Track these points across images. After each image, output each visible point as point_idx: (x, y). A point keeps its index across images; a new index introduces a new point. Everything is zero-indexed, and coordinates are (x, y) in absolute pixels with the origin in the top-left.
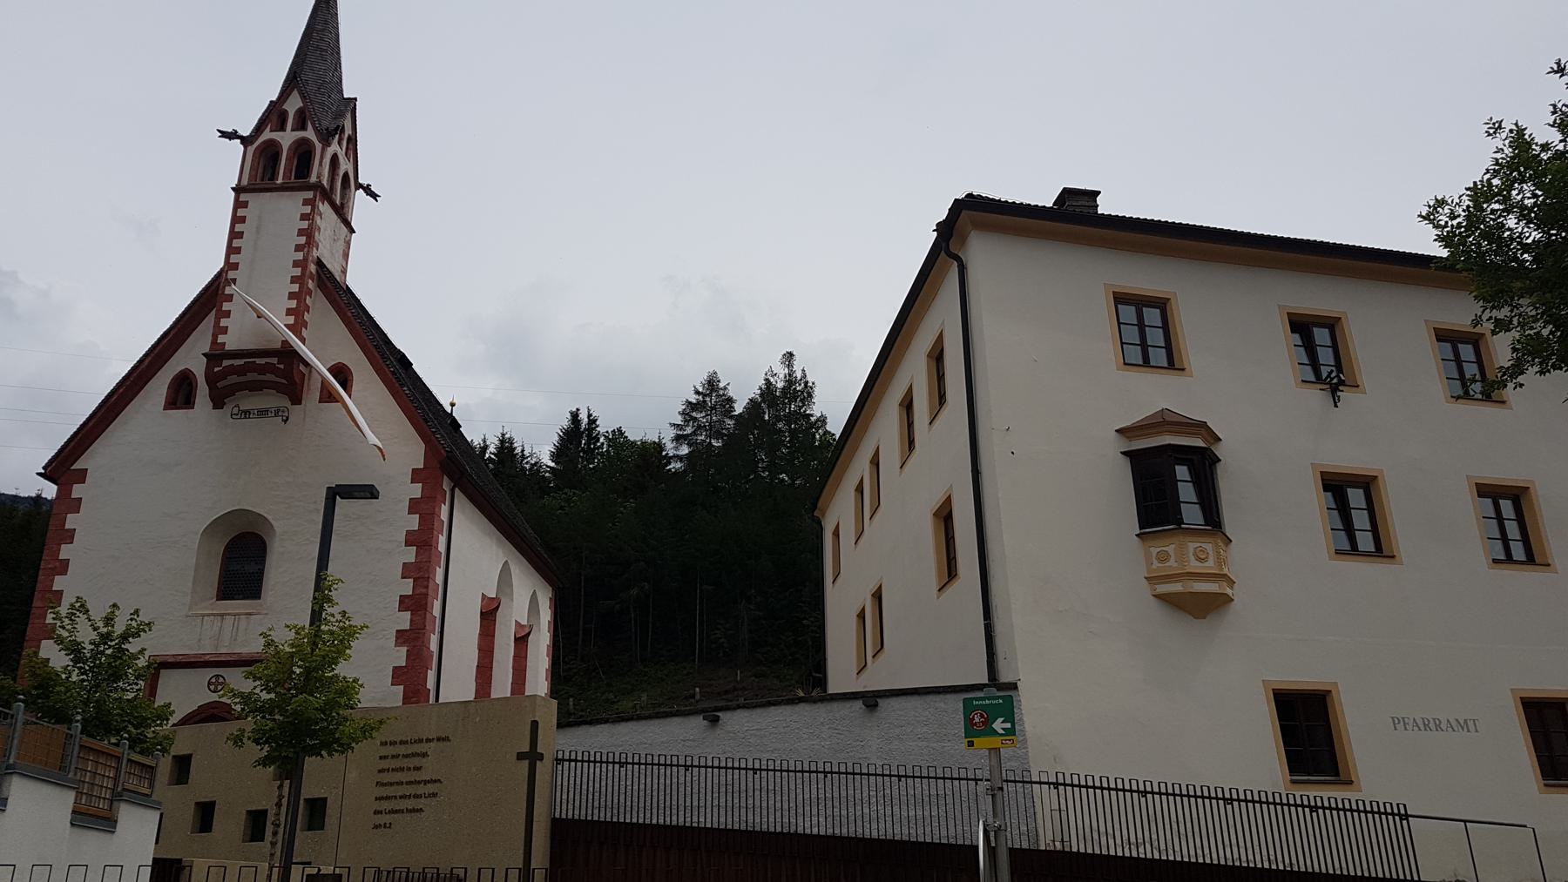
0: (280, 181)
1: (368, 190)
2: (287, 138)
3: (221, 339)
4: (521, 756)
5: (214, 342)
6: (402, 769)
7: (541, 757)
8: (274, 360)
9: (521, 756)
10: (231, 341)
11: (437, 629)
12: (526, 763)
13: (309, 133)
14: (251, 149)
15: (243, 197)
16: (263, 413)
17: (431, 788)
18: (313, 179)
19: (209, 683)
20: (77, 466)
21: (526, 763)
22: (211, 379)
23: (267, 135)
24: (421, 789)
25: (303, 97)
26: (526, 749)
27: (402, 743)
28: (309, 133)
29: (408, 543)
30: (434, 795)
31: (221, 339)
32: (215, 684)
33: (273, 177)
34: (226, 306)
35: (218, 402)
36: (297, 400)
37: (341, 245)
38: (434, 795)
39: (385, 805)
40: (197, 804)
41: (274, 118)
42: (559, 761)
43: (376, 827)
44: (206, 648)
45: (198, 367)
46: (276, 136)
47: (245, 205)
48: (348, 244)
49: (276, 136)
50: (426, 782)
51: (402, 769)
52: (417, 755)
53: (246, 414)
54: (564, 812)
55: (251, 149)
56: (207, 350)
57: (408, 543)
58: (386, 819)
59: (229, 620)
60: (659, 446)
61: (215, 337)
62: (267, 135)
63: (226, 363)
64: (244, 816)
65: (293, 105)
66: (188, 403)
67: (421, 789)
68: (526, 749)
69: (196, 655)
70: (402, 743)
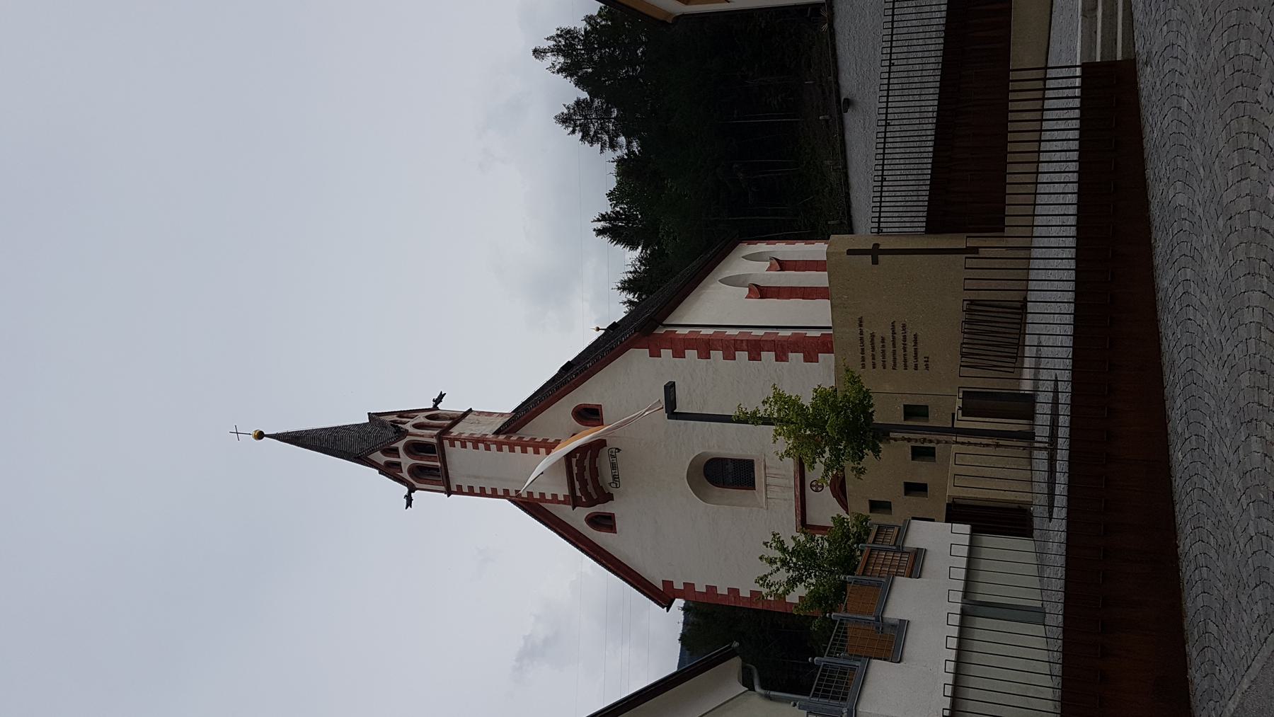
3: (561, 498)
4: (875, 262)
5: (563, 503)
7: (876, 245)
9: (875, 262)
10: (563, 491)
13: (400, 445)
14: (417, 485)
15: (454, 489)
16: (614, 466)
17: (899, 329)
18: (434, 441)
24: (899, 337)
27: (863, 351)
28: (400, 445)
30: (904, 326)
31: (561, 498)
32: (817, 487)
33: (437, 469)
34: (536, 496)
35: (609, 497)
38: (904, 326)
50: (894, 333)
53: (615, 478)
55: (417, 485)
56: (570, 507)
59: (770, 480)
60: (620, 162)
61: (560, 502)
63: (579, 494)
66: (610, 517)
67: (899, 337)
70: (863, 351)
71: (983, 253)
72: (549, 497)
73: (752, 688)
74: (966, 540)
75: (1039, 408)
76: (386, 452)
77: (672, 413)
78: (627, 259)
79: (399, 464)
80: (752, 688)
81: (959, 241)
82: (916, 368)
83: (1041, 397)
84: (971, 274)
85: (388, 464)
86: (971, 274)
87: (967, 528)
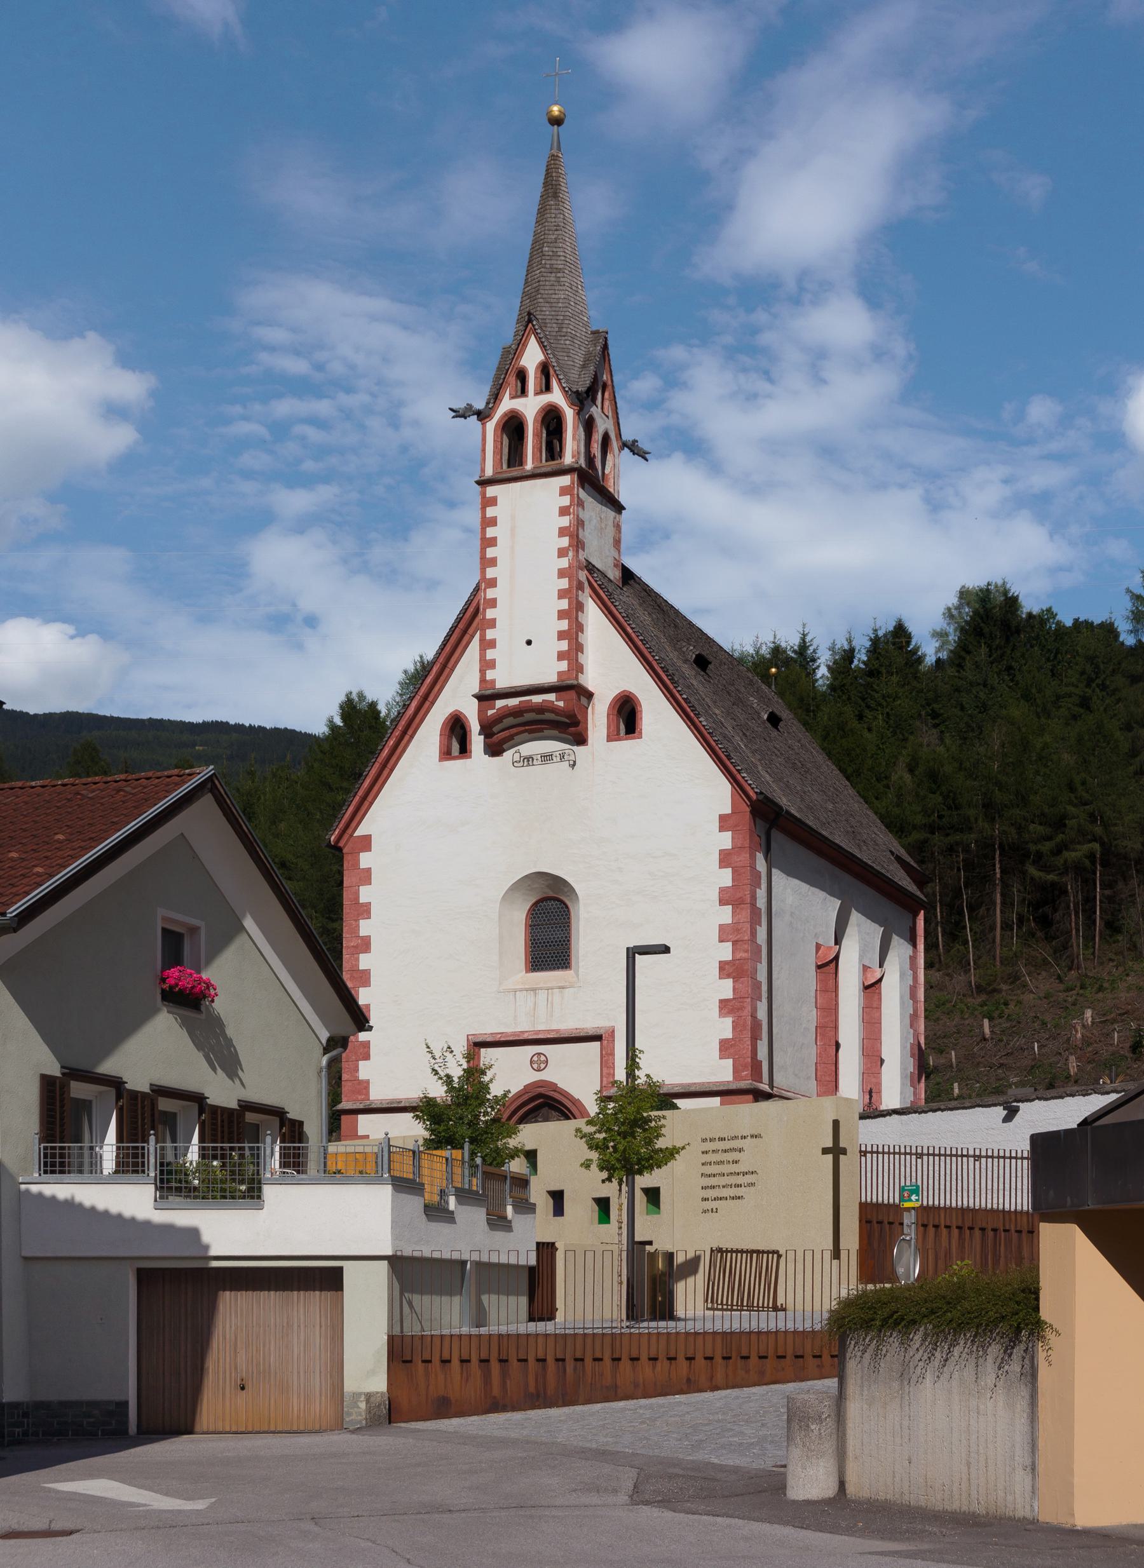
0: (529, 465)
1: (633, 447)
2: (530, 407)
3: (490, 675)
4: (825, 1151)
5: (483, 680)
6: (722, 1162)
7: (844, 1151)
8: (551, 697)
9: (825, 1151)
10: (502, 679)
11: (765, 995)
12: (830, 1156)
13: (557, 397)
14: (491, 425)
15: (491, 491)
16: (547, 758)
17: (749, 1179)
18: (568, 459)
19: (531, 1062)
20: (359, 832)
21: (830, 1156)
22: (487, 729)
23: (507, 404)
24: (740, 1180)
25: (543, 347)
26: (830, 1144)
27: (722, 1139)
28: (557, 397)
29: (722, 902)
30: (753, 1184)
31: (490, 675)
32: (539, 1063)
33: (521, 463)
34: (490, 634)
35: (494, 750)
36: (580, 740)
37: (610, 531)
38: (753, 1184)
39: (711, 1193)
40: (370, 836)
41: (512, 379)
42: (864, 1153)
43: (705, 1212)
44: (523, 1026)
45: (471, 713)
46: (519, 404)
47: (493, 502)
48: (618, 527)
49: (519, 404)
50: (745, 1173)
51: (722, 1162)
52: (734, 1150)
53: (529, 760)
54: (873, 1197)
55: (491, 425)
56: (476, 690)
57: (722, 902)
58: (714, 1205)
59: (542, 995)
60: (1108, 630)
61: (483, 673)
62: (507, 404)
63: (500, 703)
64: (590, 741)
65: (532, 357)
66: (464, 750)
67: (740, 1180)
68: (830, 1144)
69: (514, 1034)
70: (722, 1139)
71: (835, 1262)
72: (490, 654)
73: (326, 1050)
74: (523, 1262)
75: (662, 1324)
76: (545, 370)
77: (633, 953)
78: (930, 629)
79: (523, 392)
80: (326, 1050)
81: (851, 1240)
82: (706, 1199)
83: (672, 1324)
84: (818, 1256)
85: (522, 376)
86: (818, 1256)
87: (533, 1262)
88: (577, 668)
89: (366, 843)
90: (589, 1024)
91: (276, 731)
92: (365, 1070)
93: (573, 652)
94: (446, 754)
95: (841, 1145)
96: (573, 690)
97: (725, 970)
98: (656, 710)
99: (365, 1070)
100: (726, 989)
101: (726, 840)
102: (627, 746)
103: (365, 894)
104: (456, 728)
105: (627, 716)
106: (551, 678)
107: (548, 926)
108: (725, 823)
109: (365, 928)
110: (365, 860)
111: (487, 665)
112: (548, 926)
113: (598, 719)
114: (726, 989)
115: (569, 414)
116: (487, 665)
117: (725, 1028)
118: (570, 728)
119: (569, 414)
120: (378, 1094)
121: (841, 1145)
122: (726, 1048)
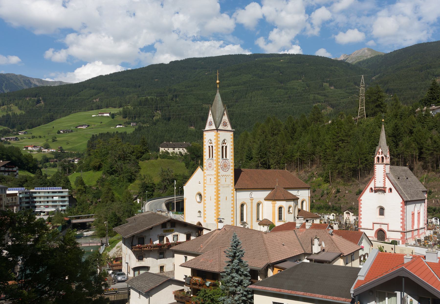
10: (377, 186)
13: (383, 155)
76: (382, 152)
88: (385, 185)
89: (361, 200)
90: (386, 223)
91: (235, 55)
92: (361, 224)
93: (384, 184)
94: (370, 192)
95: (176, 255)
96: (385, 188)
97: (401, 219)
98: (394, 190)
99: (361, 224)
100: (401, 221)
101: (401, 205)
102: (390, 193)
103: (361, 206)
104: (371, 189)
105: (391, 190)
106: (382, 186)
107: (382, 211)
108: (401, 203)
109: (361, 209)
110: (361, 202)
111: (375, 184)
112: (382, 211)
113: (387, 190)
114: (401, 221)
115: (384, 157)
116: (375, 184)
117: (401, 225)
118: (384, 191)
119: (384, 157)
120: (363, 227)
121: (176, 255)
122: (401, 227)
